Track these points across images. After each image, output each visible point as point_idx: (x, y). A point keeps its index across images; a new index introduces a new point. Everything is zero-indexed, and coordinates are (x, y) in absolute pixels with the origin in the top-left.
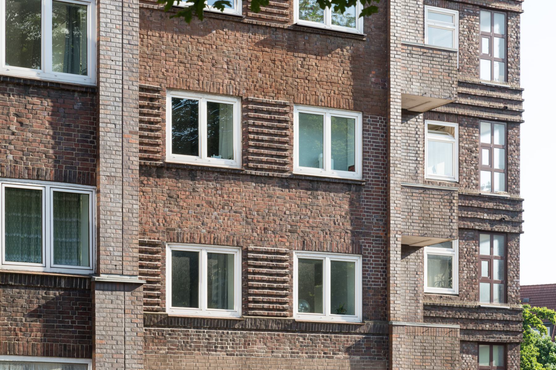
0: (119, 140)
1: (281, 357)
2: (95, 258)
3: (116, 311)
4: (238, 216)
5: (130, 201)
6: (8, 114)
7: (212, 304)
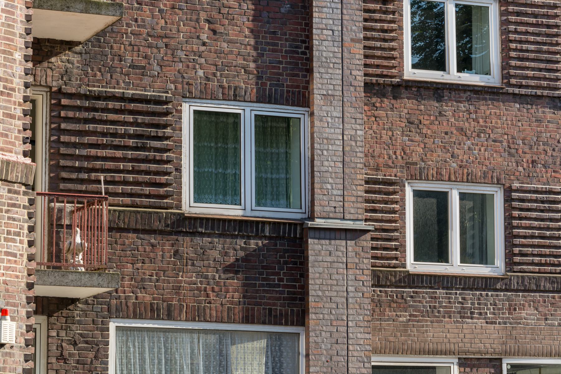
0: (338, 50)
1: (558, 326)
2: (309, 198)
3: (336, 265)
4: (498, 146)
5: (353, 125)
6: (197, 21)
7: (465, 258)
